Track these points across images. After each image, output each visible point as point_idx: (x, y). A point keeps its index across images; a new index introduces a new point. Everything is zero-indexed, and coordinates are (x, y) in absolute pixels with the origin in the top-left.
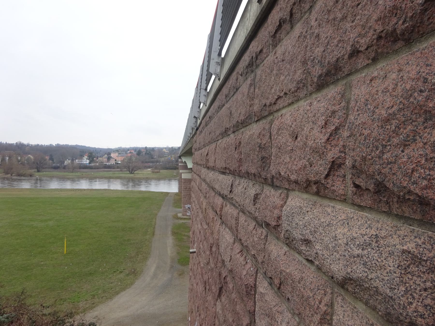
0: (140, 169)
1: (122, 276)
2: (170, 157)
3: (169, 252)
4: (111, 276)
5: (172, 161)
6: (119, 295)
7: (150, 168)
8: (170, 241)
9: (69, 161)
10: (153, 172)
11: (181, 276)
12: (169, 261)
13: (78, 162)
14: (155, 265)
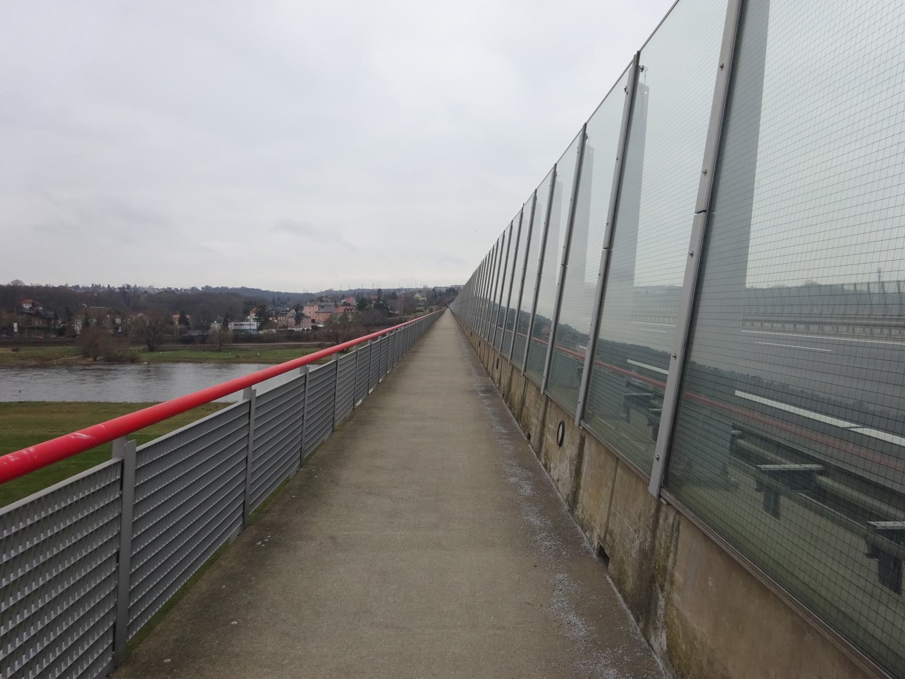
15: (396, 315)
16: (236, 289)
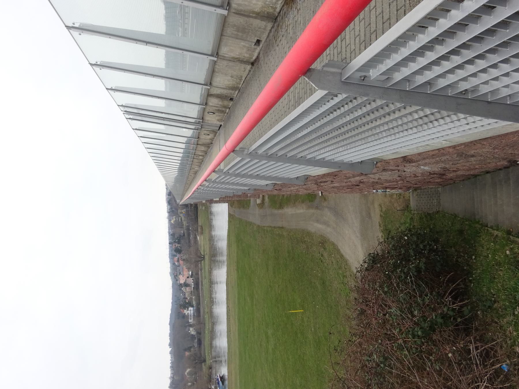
0: (198, 249)
1: (325, 254)
2: (181, 215)
3: (301, 211)
4: (326, 265)
5: (187, 212)
6: (344, 254)
7: (197, 238)
8: (289, 211)
9: (191, 329)
10: (202, 233)
11: (326, 198)
12: (312, 211)
13: (192, 319)
14: (316, 224)
15: (184, 232)
16: (170, 328)
